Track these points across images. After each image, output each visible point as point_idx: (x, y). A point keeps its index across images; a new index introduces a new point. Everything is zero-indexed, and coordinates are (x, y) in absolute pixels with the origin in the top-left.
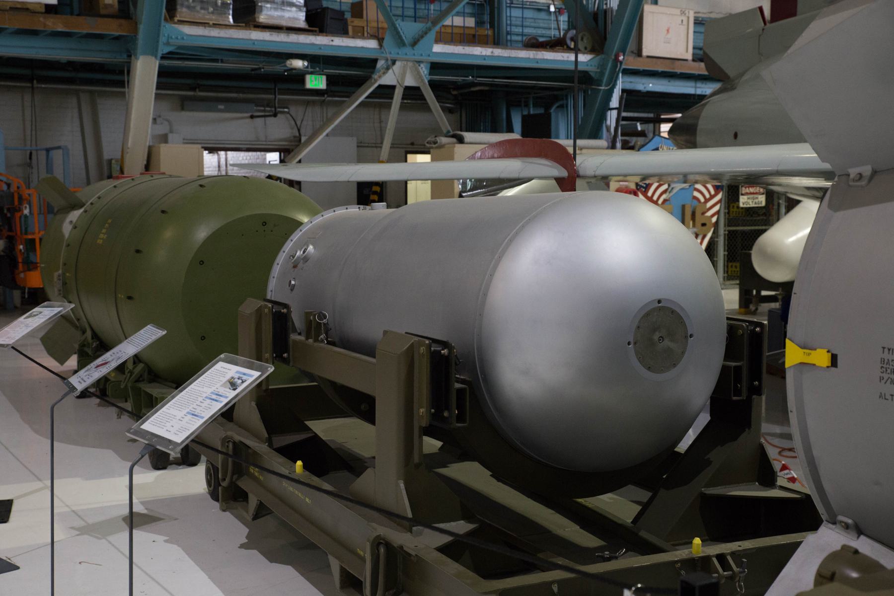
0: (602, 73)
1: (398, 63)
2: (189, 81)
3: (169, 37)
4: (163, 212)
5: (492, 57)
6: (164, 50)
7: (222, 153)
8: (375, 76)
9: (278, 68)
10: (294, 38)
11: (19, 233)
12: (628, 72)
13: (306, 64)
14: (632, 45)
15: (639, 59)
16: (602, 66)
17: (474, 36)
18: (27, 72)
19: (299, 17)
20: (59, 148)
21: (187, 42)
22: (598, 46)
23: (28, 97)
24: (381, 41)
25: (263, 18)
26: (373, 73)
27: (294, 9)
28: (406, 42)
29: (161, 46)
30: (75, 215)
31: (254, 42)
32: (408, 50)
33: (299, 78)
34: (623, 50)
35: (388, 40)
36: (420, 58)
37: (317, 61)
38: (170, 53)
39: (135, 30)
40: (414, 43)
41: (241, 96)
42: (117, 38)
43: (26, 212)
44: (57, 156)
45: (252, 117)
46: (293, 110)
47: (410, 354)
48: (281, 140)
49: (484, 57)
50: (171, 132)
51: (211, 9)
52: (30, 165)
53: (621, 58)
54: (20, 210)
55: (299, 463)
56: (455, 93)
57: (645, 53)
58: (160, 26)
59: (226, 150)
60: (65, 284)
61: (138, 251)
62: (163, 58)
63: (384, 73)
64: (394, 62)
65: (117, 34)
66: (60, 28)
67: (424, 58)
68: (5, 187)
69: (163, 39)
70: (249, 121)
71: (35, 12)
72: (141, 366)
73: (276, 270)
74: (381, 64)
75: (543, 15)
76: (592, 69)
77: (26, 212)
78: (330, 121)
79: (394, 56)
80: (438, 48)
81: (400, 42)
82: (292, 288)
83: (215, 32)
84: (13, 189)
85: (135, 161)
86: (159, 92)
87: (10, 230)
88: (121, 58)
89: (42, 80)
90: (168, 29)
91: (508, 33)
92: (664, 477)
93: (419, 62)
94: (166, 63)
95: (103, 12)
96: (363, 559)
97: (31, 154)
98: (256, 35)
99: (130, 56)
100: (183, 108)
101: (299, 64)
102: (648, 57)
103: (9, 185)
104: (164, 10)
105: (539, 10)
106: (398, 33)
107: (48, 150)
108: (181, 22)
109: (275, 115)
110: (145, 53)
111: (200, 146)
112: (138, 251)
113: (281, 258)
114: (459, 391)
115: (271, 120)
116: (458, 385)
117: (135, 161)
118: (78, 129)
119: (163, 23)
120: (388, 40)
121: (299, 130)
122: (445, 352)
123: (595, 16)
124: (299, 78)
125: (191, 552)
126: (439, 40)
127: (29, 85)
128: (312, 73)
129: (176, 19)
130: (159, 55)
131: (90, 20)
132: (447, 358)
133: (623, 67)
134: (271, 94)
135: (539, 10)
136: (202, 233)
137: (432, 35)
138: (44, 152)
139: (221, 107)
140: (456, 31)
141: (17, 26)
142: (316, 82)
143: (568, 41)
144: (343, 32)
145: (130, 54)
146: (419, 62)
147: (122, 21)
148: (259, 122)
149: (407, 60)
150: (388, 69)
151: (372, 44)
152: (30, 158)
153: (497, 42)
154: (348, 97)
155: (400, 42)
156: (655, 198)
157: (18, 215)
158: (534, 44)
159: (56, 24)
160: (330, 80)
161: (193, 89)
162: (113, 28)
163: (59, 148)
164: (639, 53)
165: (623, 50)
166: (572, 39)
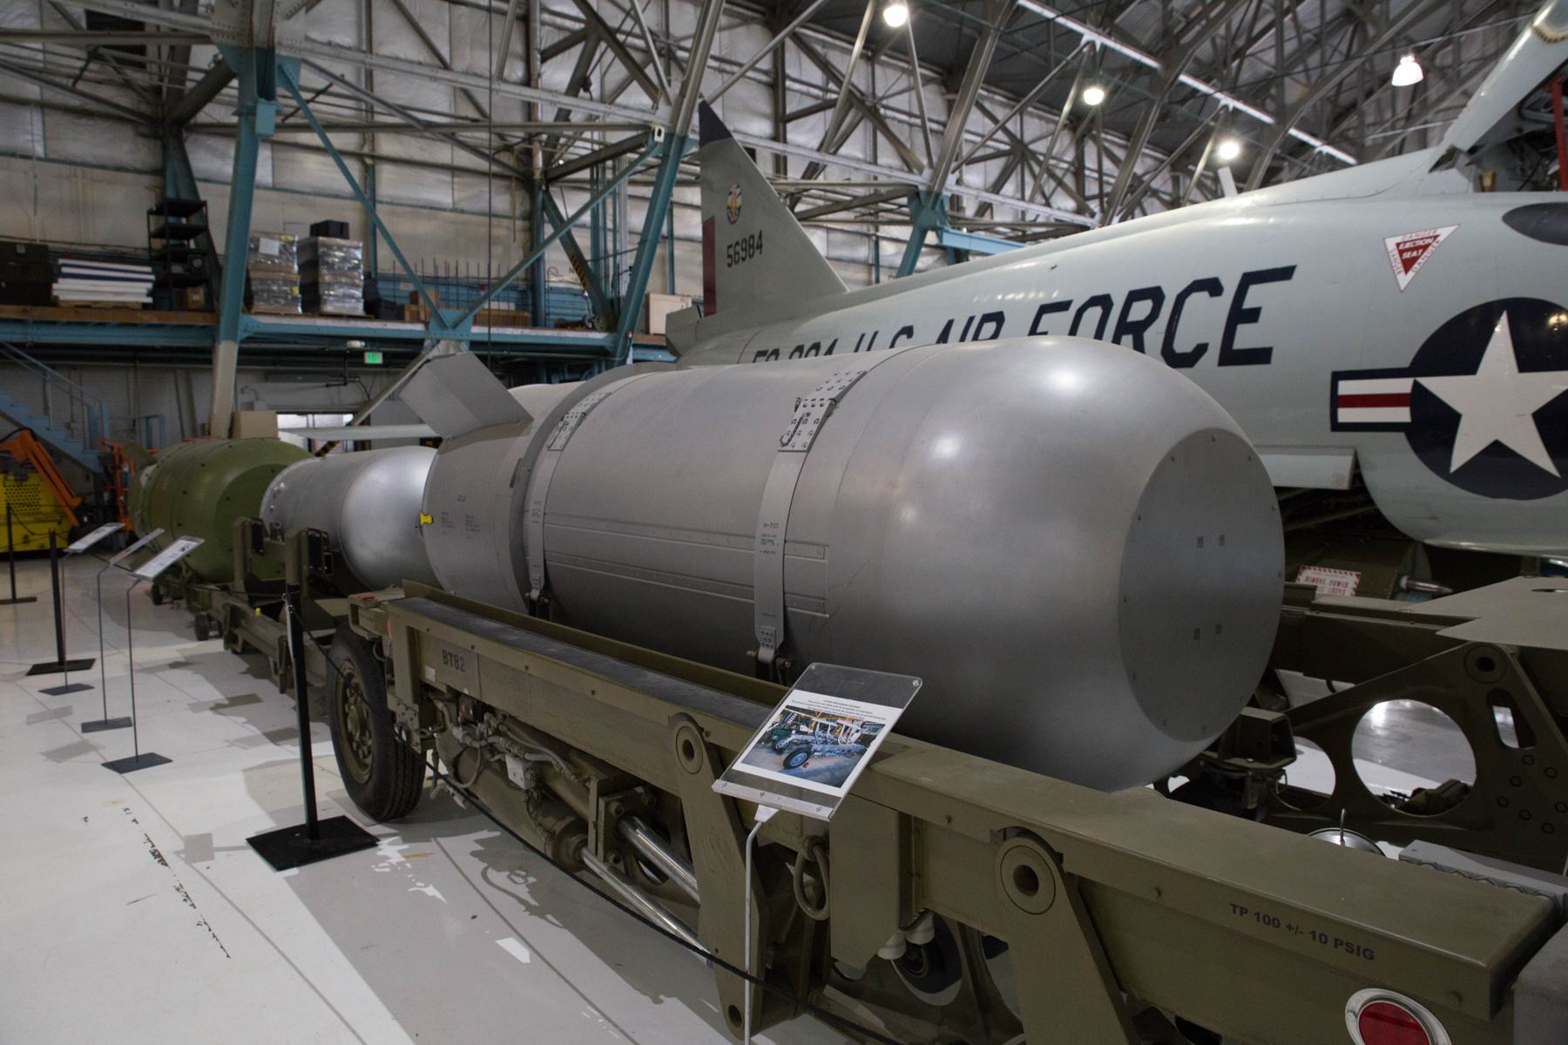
0: (616, 347)
1: (442, 343)
2: (271, 358)
3: (247, 325)
4: (203, 465)
5: (522, 336)
6: (242, 335)
7: (310, 416)
8: (423, 352)
9: (341, 348)
10: (352, 324)
11: (119, 485)
12: (636, 346)
13: (363, 344)
14: (639, 324)
15: (647, 336)
16: (616, 343)
17: (515, 317)
18: (130, 354)
19: (359, 308)
20: (155, 416)
21: (262, 329)
22: (612, 326)
23: (131, 375)
24: (426, 324)
25: (329, 308)
26: (422, 349)
27: (353, 301)
28: (448, 324)
29: (239, 332)
30: (150, 470)
31: (318, 328)
32: (450, 332)
33: (359, 354)
34: (632, 330)
35: (433, 324)
36: (460, 338)
37: (374, 342)
38: (247, 338)
39: (218, 321)
40: (455, 326)
41: (317, 369)
42: (204, 327)
43: (126, 469)
44: (155, 422)
45: (327, 386)
46: (363, 379)
47: (299, 535)
48: (354, 404)
49: (516, 336)
50: (257, 399)
51: (283, 302)
52: (133, 431)
53: (630, 335)
54: (120, 468)
55: (258, 610)
56: (501, 363)
57: (652, 331)
58: (238, 317)
59: (313, 413)
60: (143, 520)
61: (185, 492)
62: (242, 342)
63: (431, 350)
64: (438, 341)
65: (203, 324)
66: (155, 321)
67: (465, 337)
68: (109, 450)
69: (241, 327)
70: (325, 389)
71: (133, 310)
72: (190, 573)
73: (266, 500)
74: (427, 343)
75: (578, 299)
76: (608, 344)
77: (126, 469)
78: (387, 389)
79: (438, 336)
80: (476, 330)
81: (443, 325)
82: (272, 510)
83: (285, 321)
84: (115, 451)
85: (220, 426)
86: (240, 367)
87: (113, 484)
88: (206, 343)
89: (144, 360)
90: (245, 319)
91: (548, 314)
92: (1343, 811)
93: (460, 341)
94: (245, 346)
95: (193, 307)
96: (275, 650)
97: (134, 422)
98: (320, 323)
99: (214, 341)
100: (267, 380)
101: (357, 344)
102: (656, 334)
103: (112, 448)
104: (242, 303)
105: (575, 295)
106: (441, 319)
107: (148, 418)
108: (258, 313)
109: (345, 384)
110: (227, 338)
111: (274, 411)
112: (185, 492)
113: (268, 493)
114: (327, 557)
115: (342, 388)
116: (326, 553)
117: (220, 426)
118: (174, 403)
119: (241, 315)
120: (433, 324)
121: (369, 396)
122: (318, 535)
123: (612, 301)
124: (359, 354)
125: (207, 678)
126: (475, 323)
127: (132, 364)
128: (370, 351)
129: (253, 311)
130: (239, 339)
131: (180, 314)
132: (318, 539)
133: (633, 342)
134: (494, 334)
135: (575, 295)
136: (229, 478)
137: (471, 318)
138: (144, 421)
139: (300, 378)
140: (493, 313)
141: (117, 321)
142: (374, 358)
143: (587, 322)
144: (399, 317)
145: (215, 339)
146: (460, 341)
147: (207, 314)
148: (333, 390)
149: (450, 340)
150: (433, 346)
151: (419, 327)
152: (134, 425)
153: (535, 323)
154: (404, 367)
155: (443, 325)
156: (1346, 415)
157: (119, 472)
158: (563, 325)
159: (152, 318)
160: (385, 355)
161: (274, 363)
162: (199, 320)
163: (155, 416)
164: (647, 331)
165: (632, 330)
166: (590, 321)
